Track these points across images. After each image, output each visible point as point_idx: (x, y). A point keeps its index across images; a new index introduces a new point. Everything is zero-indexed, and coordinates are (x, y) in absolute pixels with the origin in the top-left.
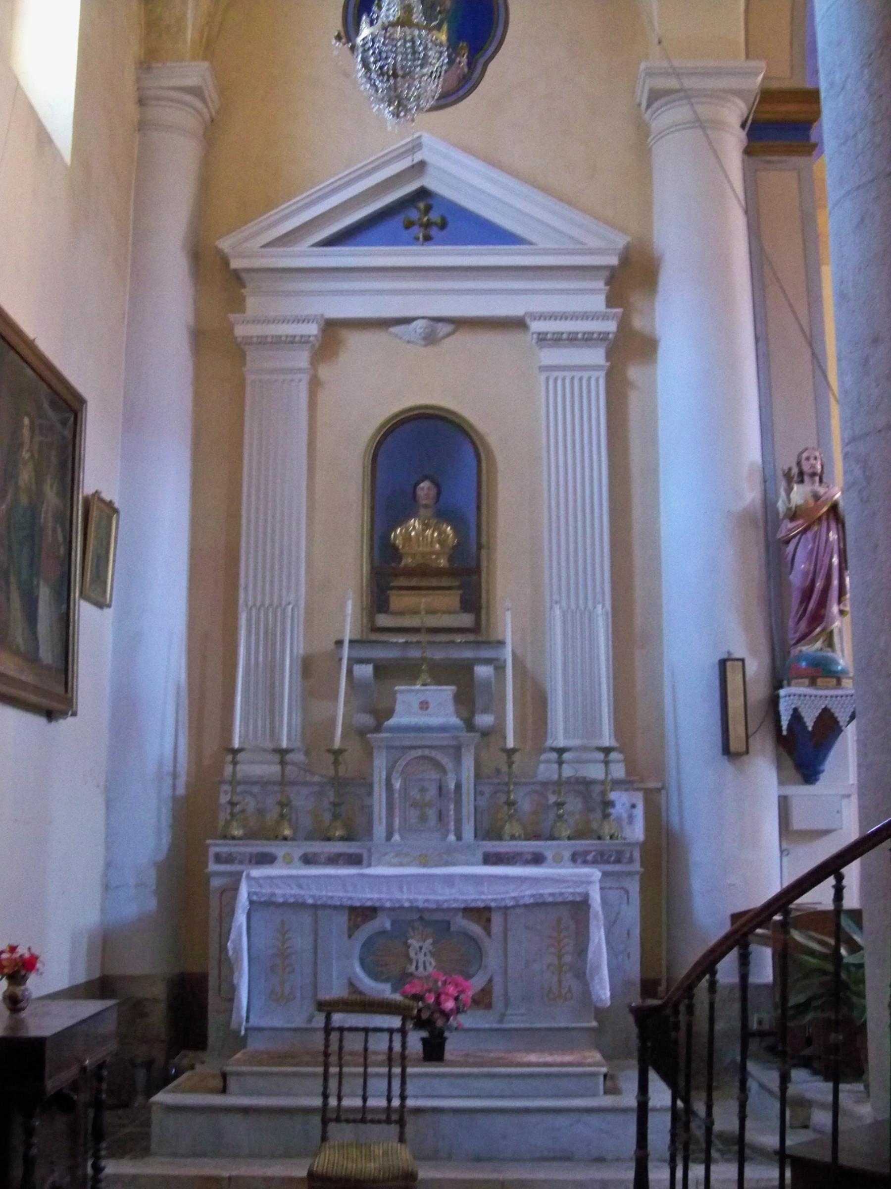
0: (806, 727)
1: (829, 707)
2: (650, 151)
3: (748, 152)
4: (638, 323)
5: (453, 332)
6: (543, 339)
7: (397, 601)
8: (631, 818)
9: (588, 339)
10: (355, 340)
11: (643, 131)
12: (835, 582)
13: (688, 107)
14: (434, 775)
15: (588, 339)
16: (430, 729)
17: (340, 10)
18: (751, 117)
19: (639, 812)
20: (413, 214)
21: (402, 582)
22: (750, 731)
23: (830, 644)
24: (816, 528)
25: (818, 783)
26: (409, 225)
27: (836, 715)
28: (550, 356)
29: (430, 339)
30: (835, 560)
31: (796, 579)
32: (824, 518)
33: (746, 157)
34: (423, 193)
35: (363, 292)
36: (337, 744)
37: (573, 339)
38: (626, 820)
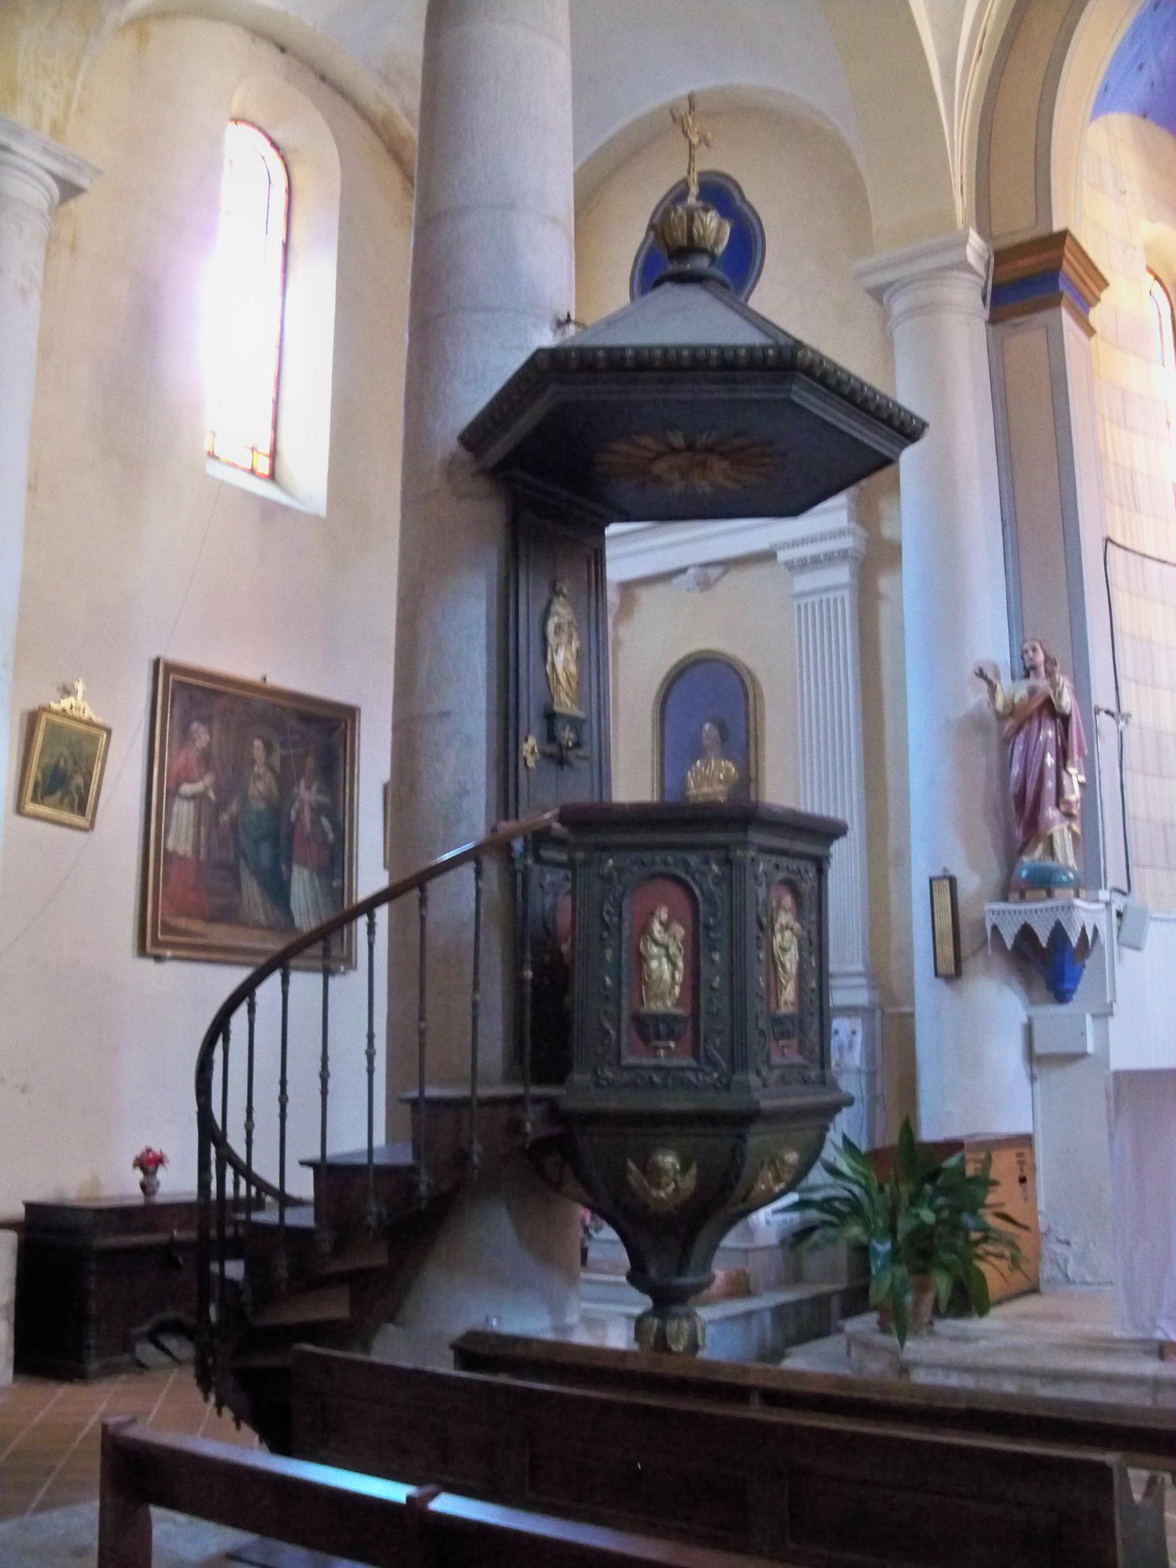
0: (1040, 945)
1: (1029, 922)
4: (887, 531)
5: (725, 573)
6: (790, 565)
8: (851, 1045)
9: (829, 559)
10: (646, 597)
12: (1050, 784)
15: (829, 559)
17: (628, 282)
18: (990, 282)
19: (858, 1039)
22: (965, 950)
23: (1051, 851)
24: (1026, 727)
25: (1070, 1005)
27: (1036, 930)
28: (804, 582)
29: (705, 585)
30: (1050, 760)
31: (1013, 789)
32: (1035, 714)
33: (990, 328)
35: (644, 551)
37: (816, 562)
38: (846, 1047)
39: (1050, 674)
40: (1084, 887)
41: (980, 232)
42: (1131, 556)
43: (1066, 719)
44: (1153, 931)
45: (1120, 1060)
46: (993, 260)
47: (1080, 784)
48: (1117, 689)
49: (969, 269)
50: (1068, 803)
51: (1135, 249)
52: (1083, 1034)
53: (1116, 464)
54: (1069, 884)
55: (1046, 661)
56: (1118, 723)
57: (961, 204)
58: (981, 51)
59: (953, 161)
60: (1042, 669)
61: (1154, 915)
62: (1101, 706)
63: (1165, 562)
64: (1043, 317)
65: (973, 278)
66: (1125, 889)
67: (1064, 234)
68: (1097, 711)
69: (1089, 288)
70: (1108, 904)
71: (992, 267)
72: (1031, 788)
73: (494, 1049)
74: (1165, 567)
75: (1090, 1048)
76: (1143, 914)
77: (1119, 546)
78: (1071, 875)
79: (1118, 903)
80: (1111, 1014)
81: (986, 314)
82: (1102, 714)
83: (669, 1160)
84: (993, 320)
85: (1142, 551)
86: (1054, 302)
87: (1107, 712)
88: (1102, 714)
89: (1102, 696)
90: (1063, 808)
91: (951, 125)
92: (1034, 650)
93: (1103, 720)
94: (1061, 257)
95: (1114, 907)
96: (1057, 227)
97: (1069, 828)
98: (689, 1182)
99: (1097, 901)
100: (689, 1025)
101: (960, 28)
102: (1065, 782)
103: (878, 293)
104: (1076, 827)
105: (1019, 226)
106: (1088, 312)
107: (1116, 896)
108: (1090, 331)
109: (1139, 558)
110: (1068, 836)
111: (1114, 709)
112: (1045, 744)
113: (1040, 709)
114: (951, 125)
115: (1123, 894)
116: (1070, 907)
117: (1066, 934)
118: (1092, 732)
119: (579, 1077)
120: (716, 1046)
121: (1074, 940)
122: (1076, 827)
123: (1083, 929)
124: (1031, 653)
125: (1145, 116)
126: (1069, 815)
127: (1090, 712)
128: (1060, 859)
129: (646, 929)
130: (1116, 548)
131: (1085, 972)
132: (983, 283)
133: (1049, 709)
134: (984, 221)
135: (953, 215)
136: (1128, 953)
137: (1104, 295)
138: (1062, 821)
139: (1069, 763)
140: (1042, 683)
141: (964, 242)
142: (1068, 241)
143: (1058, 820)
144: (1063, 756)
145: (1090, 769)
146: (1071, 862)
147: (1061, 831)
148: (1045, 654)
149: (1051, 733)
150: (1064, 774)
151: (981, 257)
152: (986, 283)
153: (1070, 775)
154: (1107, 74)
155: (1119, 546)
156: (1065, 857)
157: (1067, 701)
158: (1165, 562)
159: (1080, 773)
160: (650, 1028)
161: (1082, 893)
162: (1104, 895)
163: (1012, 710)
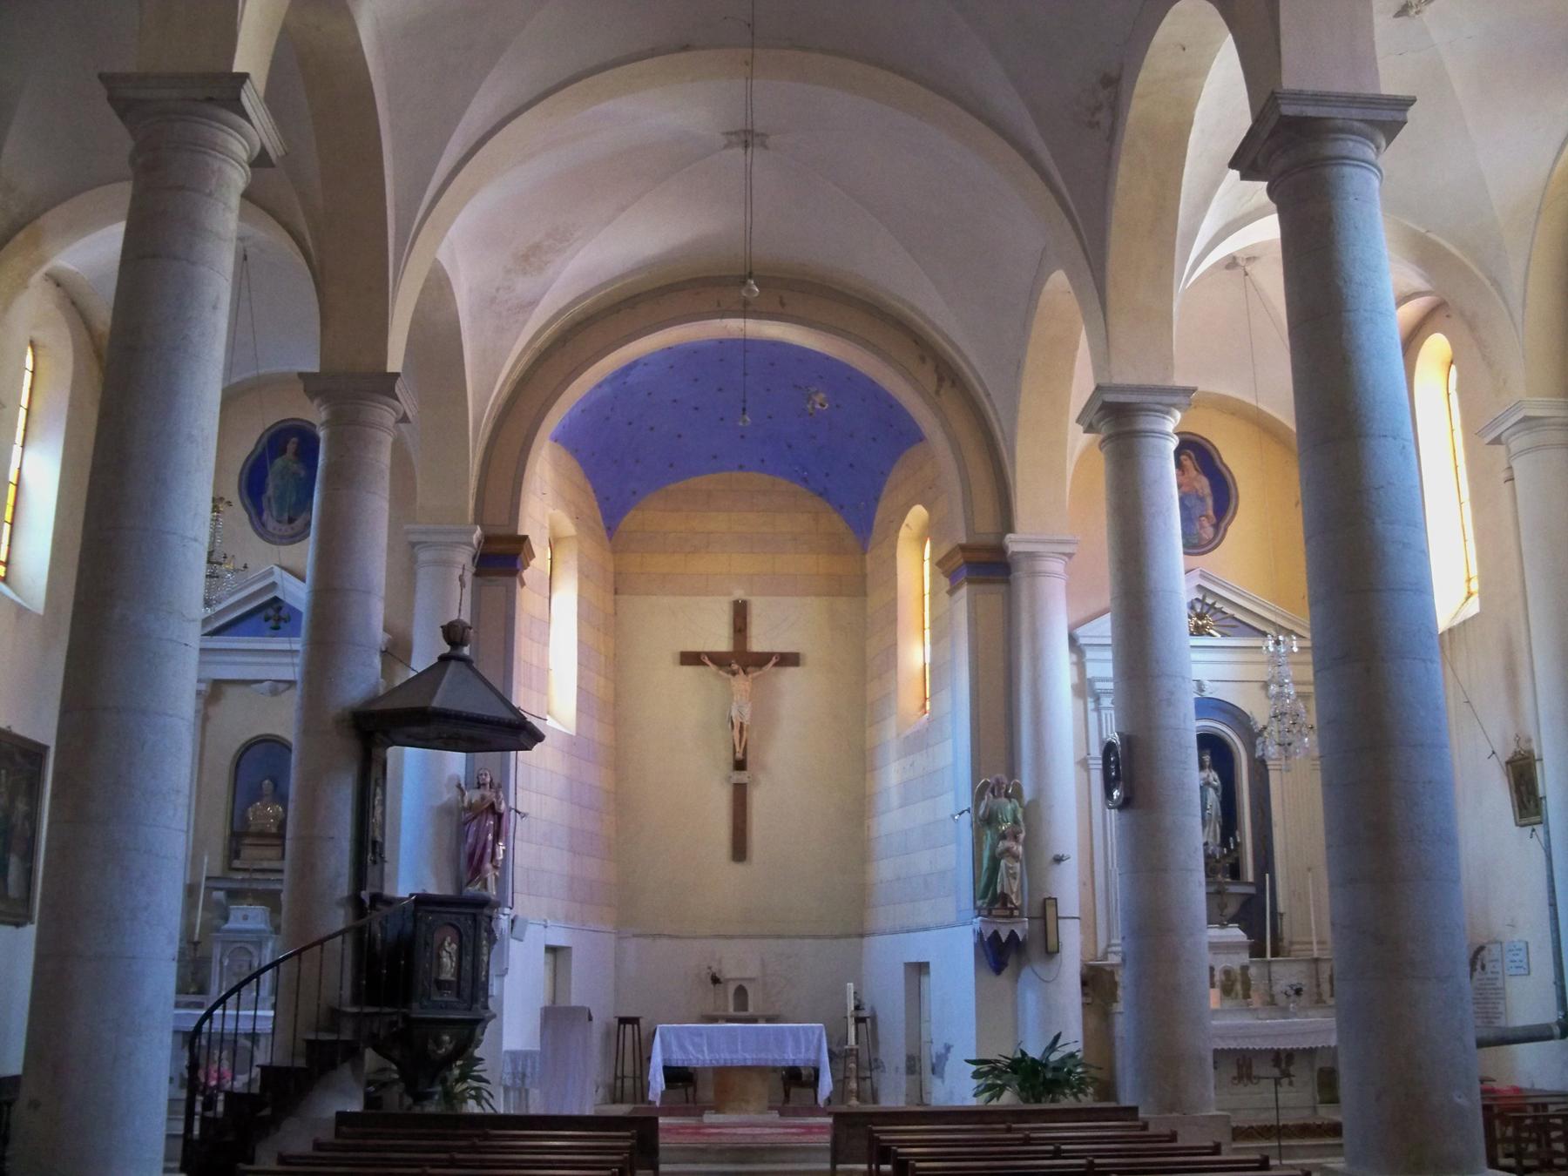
2: (415, 574)
3: (476, 574)
7: (247, 852)
11: (413, 560)
12: (489, 850)
13: (1289, 82)
14: (246, 958)
16: (247, 931)
20: (271, 612)
21: (248, 841)
23: (485, 887)
26: (267, 619)
29: (274, 692)
30: (490, 837)
31: (466, 849)
34: (276, 599)
36: (196, 938)
49: (470, 544)
67: (525, 538)
72: (478, 852)
73: (347, 992)
83: (447, 1038)
98: (450, 1047)
100: (456, 986)
103: (413, 545)
119: (415, 1005)
120: (466, 992)
126: (496, 867)
129: (442, 944)
133: (492, 809)
134: (479, 519)
140: (488, 793)
144: (497, 837)
147: (491, 875)
160: (441, 985)
163: (471, 807)
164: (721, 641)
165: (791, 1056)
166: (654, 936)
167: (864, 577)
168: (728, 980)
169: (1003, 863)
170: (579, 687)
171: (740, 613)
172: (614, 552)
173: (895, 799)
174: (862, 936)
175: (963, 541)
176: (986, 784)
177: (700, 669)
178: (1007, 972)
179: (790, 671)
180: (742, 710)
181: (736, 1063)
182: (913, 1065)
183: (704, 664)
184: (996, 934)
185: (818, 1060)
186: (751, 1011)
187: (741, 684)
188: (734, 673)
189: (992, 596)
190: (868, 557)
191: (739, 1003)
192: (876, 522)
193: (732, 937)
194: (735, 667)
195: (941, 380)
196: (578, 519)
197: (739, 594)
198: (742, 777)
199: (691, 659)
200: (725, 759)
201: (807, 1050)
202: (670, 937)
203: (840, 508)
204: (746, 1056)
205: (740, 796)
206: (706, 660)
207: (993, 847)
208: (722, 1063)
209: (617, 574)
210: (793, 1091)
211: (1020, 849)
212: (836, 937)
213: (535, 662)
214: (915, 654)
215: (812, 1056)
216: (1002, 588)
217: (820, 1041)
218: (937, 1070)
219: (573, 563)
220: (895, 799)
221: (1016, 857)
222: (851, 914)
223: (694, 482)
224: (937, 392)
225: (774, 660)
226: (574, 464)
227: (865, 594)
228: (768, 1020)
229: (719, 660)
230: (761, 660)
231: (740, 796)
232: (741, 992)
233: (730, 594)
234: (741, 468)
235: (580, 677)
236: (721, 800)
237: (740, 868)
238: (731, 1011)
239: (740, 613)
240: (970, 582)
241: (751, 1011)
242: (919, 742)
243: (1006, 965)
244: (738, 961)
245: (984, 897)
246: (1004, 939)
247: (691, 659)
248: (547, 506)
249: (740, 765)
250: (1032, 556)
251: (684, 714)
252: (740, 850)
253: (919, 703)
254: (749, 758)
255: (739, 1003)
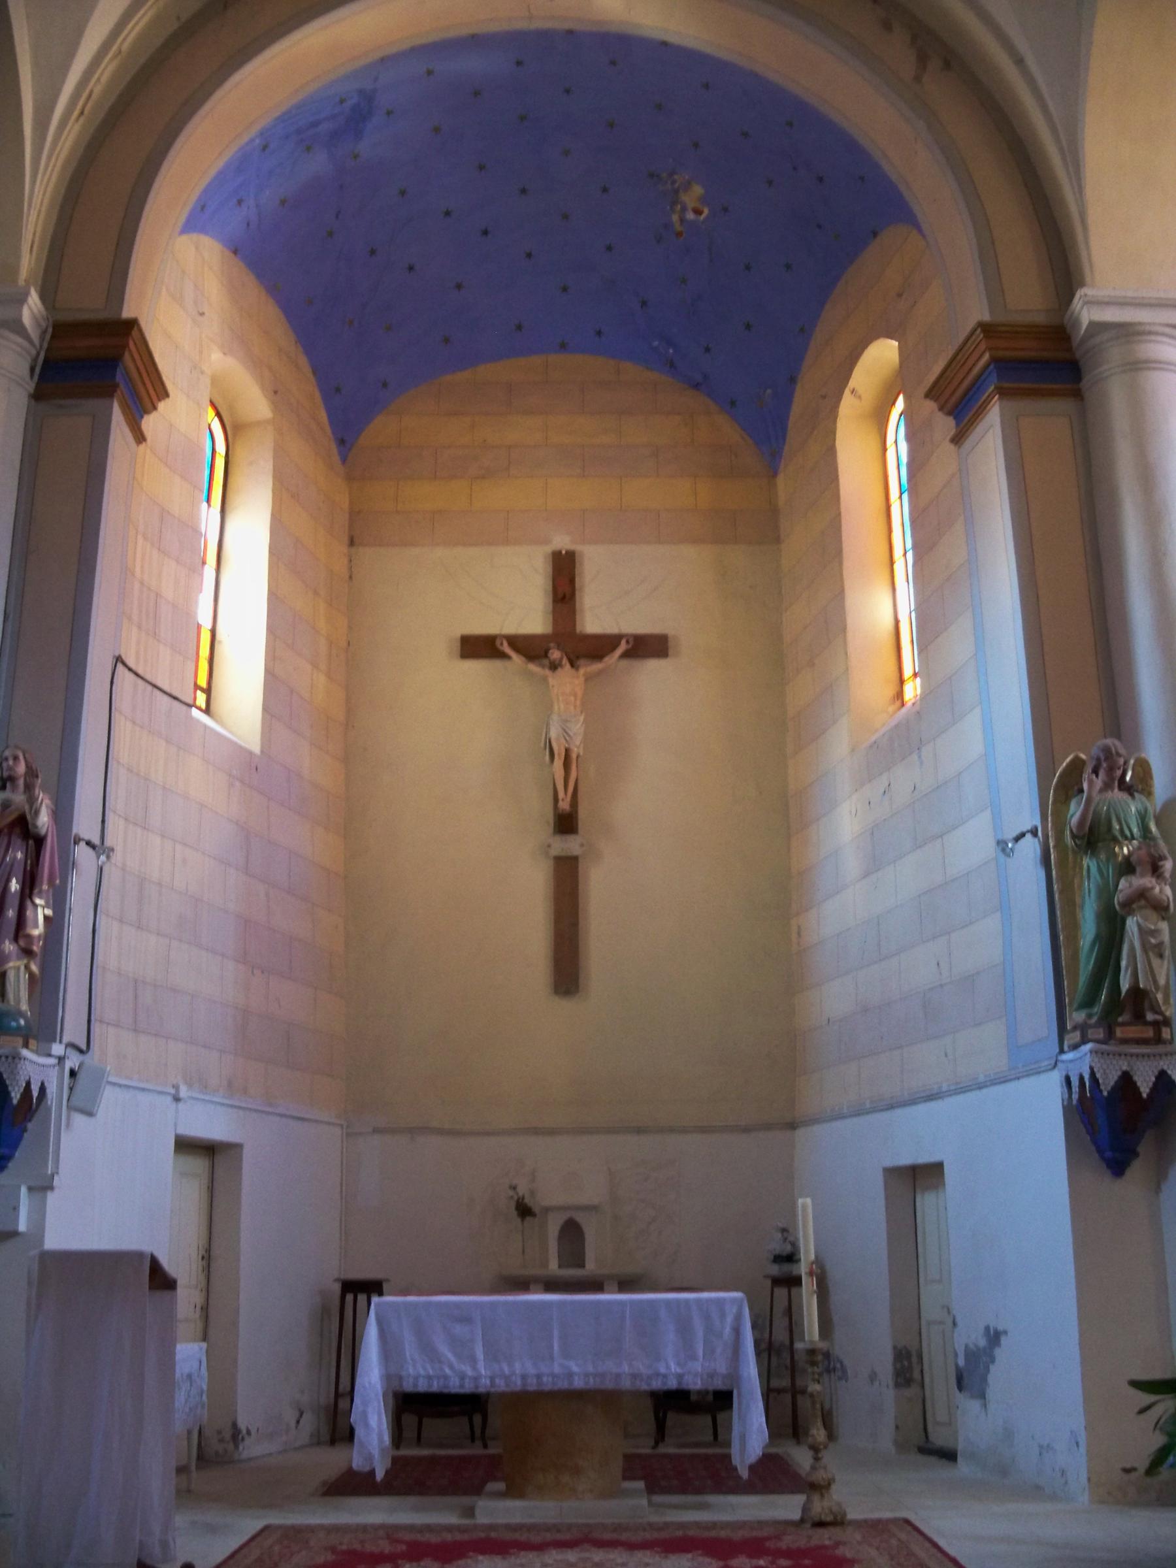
30: (14, 886)
33: (33, 402)
39: (29, 788)
40: (35, 1038)
41: (43, 297)
42: (140, 681)
43: (40, 841)
44: (110, 1100)
45: (53, 1241)
46: (50, 330)
47: (46, 918)
48: (103, 821)
49: (17, 327)
50: (29, 937)
51: (202, 372)
52: (16, 1209)
53: (142, 583)
54: (18, 1031)
55: (26, 774)
56: (98, 858)
57: (28, 262)
58: (82, 113)
59: (29, 215)
60: (21, 782)
61: (112, 1079)
62: (82, 836)
63: (175, 698)
64: (93, 404)
65: (25, 344)
66: (84, 1047)
67: (132, 324)
68: (77, 840)
69: (144, 384)
70: (61, 1059)
71: (48, 337)
74: (176, 703)
75: (22, 1227)
76: (99, 1078)
77: (130, 669)
78: (22, 1022)
79: (73, 1061)
80: (51, 1188)
81: (31, 387)
82: (82, 844)
84: (38, 396)
85: (154, 682)
86: (108, 392)
87: (88, 843)
88: (82, 844)
89: (85, 824)
90: (22, 943)
91: (33, 182)
92: (16, 758)
93: (82, 853)
94: (125, 346)
95: (68, 1065)
96: (126, 314)
97: (27, 967)
99: (50, 1055)
101: (63, 82)
102: (29, 913)
104: (34, 968)
105: (86, 304)
106: (142, 417)
107: (70, 1051)
108: (140, 438)
109: (150, 688)
110: (24, 977)
111: (96, 840)
112: (12, 865)
113: (12, 825)
114: (33, 182)
115: (81, 1051)
116: (16, 1057)
117: (6, 1087)
118: (67, 864)
121: (16, 1096)
122: (34, 968)
123: (28, 1084)
124: (11, 762)
125: (235, 252)
126: (28, 952)
127: (68, 840)
128: (12, 1003)
130: (126, 671)
131: (26, 1135)
132: (34, 352)
135: (15, 271)
136: (79, 1119)
137: (161, 406)
138: (19, 959)
139: (36, 891)
141: (22, 299)
142: (135, 333)
143: (14, 956)
145: (59, 902)
146: (24, 1007)
148: (27, 766)
149: (19, 855)
150: (29, 903)
151: (38, 324)
152: (38, 354)
153: (36, 906)
154: (206, 191)
155: (130, 669)
156: (18, 1001)
157: (43, 820)
158: (175, 698)
159: (47, 906)
161: (32, 1042)
162: (58, 1049)
164: (531, 616)
165: (679, 1366)
166: (413, 1131)
167: (774, 512)
168: (547, 1210)
169: (1131, 924)
170: (270, 673)
171: (564, 576)
172: (349, 478)
173: (852, 864)
174: (792, 1126)
175: (987, 317)
176: (1077, 767)
177: (497, 664)
178: (1137, 1170)
179: (652, 666)
180: (569, 725)
181: (548, 1384)
182: (907, 1367)
183: (503, 656)
184: (1126, 1080)
185: (734, 1375)
186: (591, 1266)
187: (567, 684)
188: (554, 667)
189: (1050, 419)
190: (780, 480)
191: (564, 1252)
192: (790, 425)
193: (551, 1132)
194: (555, 654)
195: (922, 60)
196: (276, 393)
197: (562, 542)
198: (570, 845)
199: (478, 647)
200: (540, 811)
201: (710, 1352)
202: (441, 1132)
203: (730, 405)
204: (573, 1368)
205: (567, 878)
206: (506, 648)
207: (1106, 894)
208: (517, 1385)
209: (354, 514)
210: (672, 1418)
211: (1168, 891)
212: (746, 1130)
213: (168, 592)
214: (882, 604)
215: (721, 1366)
216: (1065, 405)
217: (737, 1331)
218: (970, 1377)
219: (266, 465)
220: (852, 864)
221: (1160, 908)
222: (769, 1079)
223: (486, 371)
224: (918, 79)
225: (623, 647)
226: (272, 311)
227: (778, 540)
228: (626, 1284)
229: (530, 648)
230: (597, 648)
231: (567, 878)
232: (572, 1232)
233: (546, 541)
234: (563, 347)
235: (272, 656)
236: (533, 883)
237: (566, 1006)
238: (553, 1266)
239: (564, 576)
240: (1003, 393)
241: (591, 1266)
242: (907, 739)
243: (1135, 1154)
244: (568, 1174)
245: (1089, 1001)
246: (1145, 1091)
247: (478, 647)
248: (193, 310)
249: (566, 823)
250: (1128, 332)
251: (462, 737)
252: (567, 974)
253: (891, 691)
254: (582, 814)
255: (564, 1252)
